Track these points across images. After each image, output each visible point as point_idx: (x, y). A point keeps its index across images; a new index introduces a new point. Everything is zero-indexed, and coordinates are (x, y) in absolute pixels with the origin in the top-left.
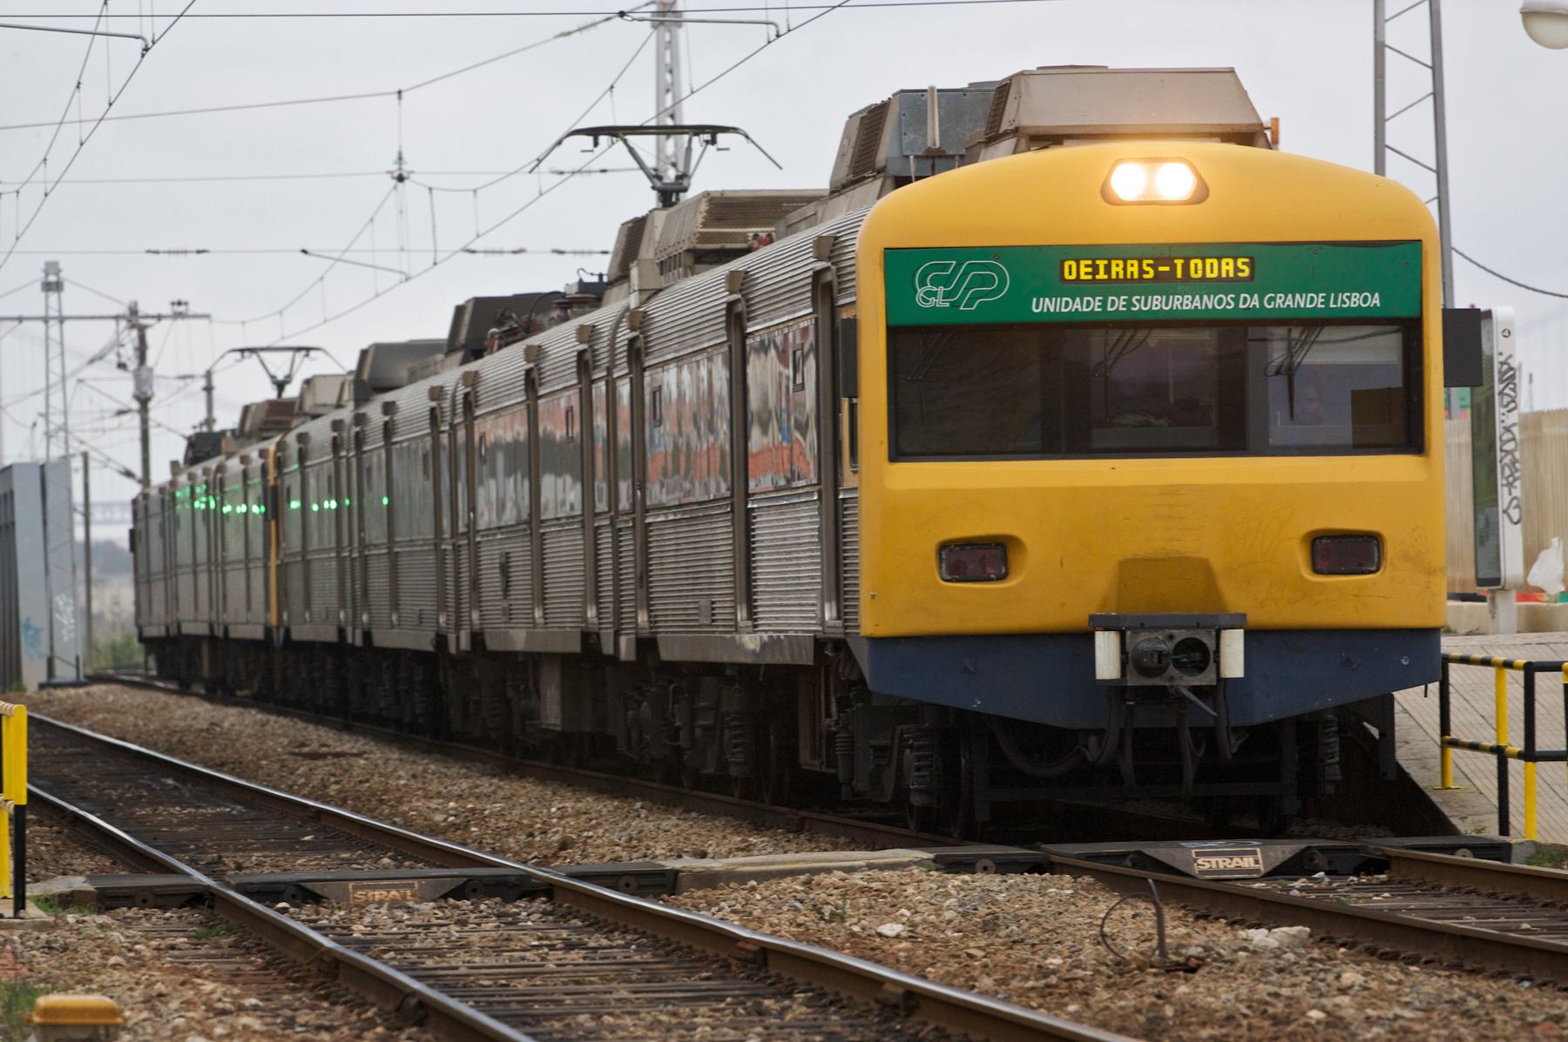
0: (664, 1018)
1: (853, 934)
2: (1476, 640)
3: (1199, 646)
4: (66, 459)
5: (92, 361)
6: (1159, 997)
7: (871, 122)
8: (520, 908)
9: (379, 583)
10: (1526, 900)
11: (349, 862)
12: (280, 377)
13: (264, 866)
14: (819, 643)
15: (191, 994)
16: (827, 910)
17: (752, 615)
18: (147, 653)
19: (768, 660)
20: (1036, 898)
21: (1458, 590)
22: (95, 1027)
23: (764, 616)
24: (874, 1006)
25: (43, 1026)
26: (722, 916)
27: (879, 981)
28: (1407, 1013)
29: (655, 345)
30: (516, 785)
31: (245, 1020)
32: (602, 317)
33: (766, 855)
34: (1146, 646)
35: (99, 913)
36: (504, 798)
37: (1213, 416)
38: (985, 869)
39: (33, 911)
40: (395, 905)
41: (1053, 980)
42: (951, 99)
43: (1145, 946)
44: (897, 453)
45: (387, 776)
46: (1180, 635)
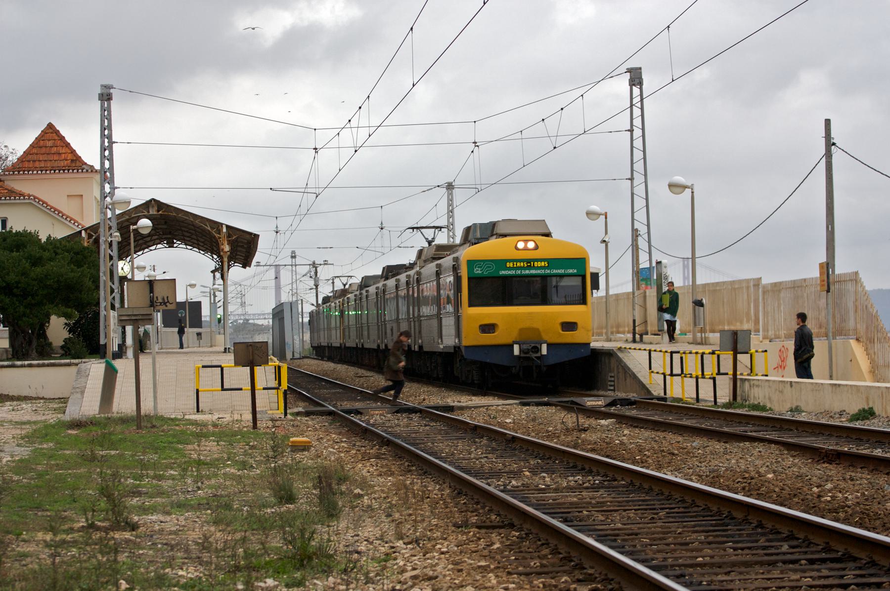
0: (450, 444)
1: (499, 422)
2: (658, 345)
3: (537, 348)
4: (297, 301)
5: (303, 276)
6: (577, 438)
7: (468, 230)
8: (413, 416)
9: (365, 333)
10: (670, 412)
11: (369, 404)
12: (430, 239)
13: (347, 405)
14: (455, 347)
15: (329, 438)
16: (492, 416)
17: (442, 341)
18: (313, 350)
19: (444, 351)
20: (546, 412)
21: (653, 333)
22: (305, 446)
23: (444, 341)
24: (504, 440)
25: (291, 446)
26: (465, 417)
27: (505, 434)
28: (640, 441)
29: (422, 279)
30: (412, 384)
31: (343, 444)
32: (411, 273)
33: (477, 401)
34: (525, 348)
35: (306, 417)
36: (409, 388)
37: (540, 297)
38: (533, 405)
39: (289, 416)
40: (381, 415)
41: (550, 433)
42: (482, 225)
43: (573, 425)
44: (470, 305)
45: (379, 382)
46: (533, 345)
